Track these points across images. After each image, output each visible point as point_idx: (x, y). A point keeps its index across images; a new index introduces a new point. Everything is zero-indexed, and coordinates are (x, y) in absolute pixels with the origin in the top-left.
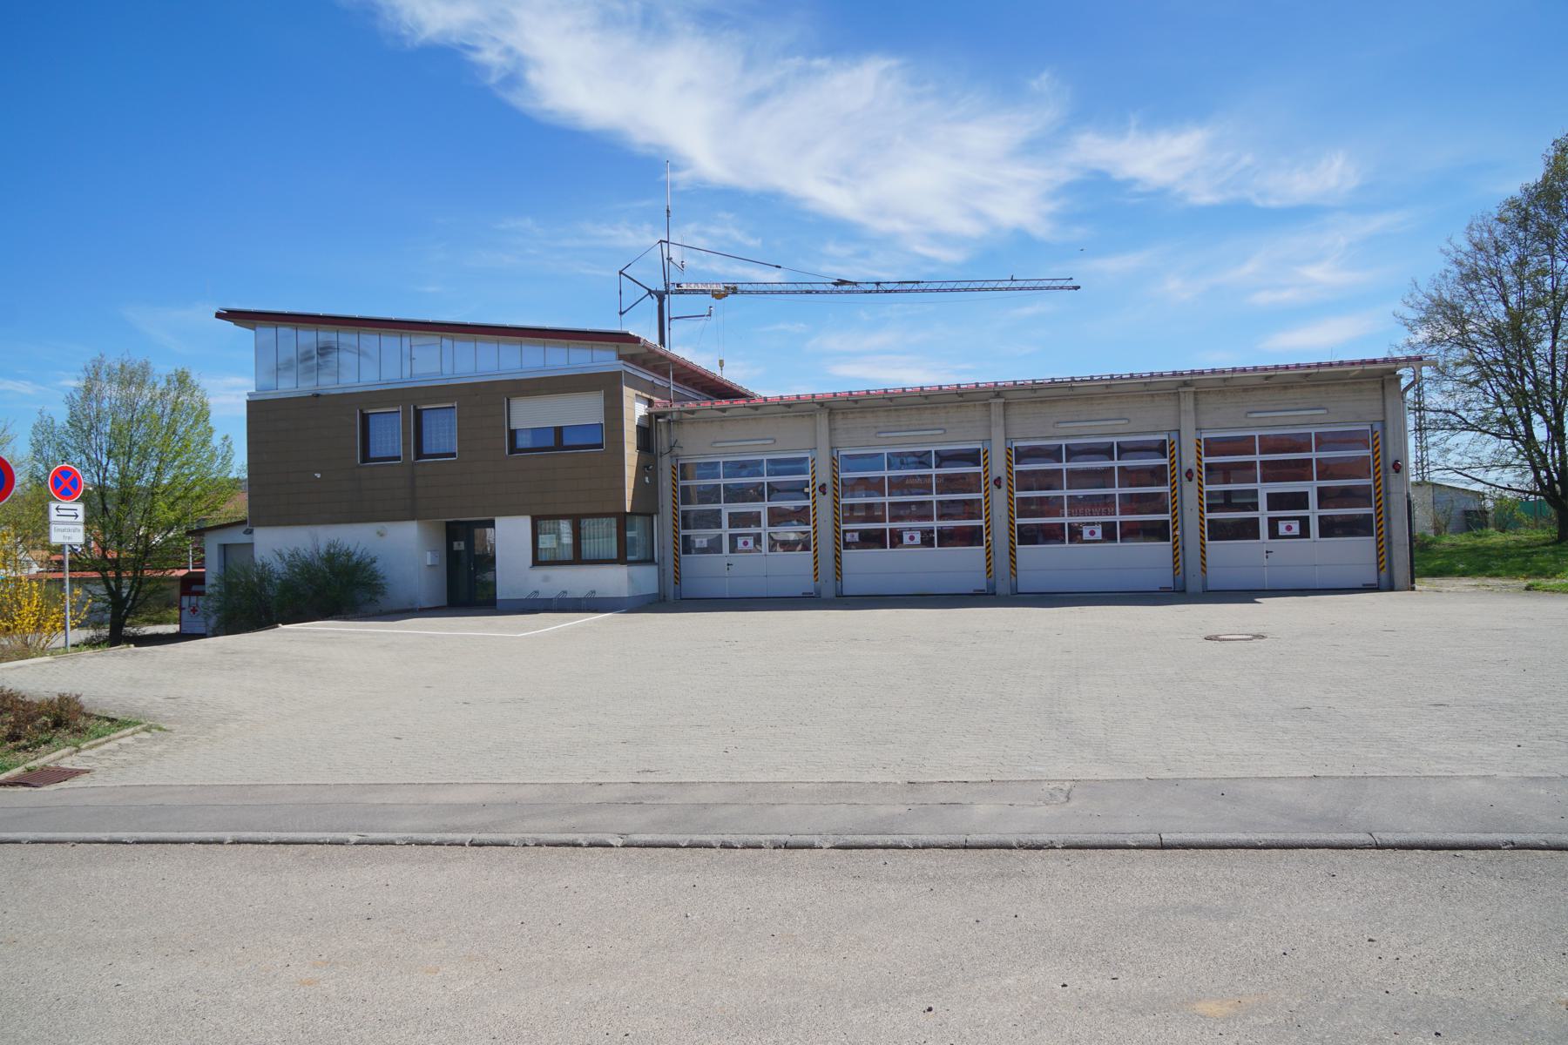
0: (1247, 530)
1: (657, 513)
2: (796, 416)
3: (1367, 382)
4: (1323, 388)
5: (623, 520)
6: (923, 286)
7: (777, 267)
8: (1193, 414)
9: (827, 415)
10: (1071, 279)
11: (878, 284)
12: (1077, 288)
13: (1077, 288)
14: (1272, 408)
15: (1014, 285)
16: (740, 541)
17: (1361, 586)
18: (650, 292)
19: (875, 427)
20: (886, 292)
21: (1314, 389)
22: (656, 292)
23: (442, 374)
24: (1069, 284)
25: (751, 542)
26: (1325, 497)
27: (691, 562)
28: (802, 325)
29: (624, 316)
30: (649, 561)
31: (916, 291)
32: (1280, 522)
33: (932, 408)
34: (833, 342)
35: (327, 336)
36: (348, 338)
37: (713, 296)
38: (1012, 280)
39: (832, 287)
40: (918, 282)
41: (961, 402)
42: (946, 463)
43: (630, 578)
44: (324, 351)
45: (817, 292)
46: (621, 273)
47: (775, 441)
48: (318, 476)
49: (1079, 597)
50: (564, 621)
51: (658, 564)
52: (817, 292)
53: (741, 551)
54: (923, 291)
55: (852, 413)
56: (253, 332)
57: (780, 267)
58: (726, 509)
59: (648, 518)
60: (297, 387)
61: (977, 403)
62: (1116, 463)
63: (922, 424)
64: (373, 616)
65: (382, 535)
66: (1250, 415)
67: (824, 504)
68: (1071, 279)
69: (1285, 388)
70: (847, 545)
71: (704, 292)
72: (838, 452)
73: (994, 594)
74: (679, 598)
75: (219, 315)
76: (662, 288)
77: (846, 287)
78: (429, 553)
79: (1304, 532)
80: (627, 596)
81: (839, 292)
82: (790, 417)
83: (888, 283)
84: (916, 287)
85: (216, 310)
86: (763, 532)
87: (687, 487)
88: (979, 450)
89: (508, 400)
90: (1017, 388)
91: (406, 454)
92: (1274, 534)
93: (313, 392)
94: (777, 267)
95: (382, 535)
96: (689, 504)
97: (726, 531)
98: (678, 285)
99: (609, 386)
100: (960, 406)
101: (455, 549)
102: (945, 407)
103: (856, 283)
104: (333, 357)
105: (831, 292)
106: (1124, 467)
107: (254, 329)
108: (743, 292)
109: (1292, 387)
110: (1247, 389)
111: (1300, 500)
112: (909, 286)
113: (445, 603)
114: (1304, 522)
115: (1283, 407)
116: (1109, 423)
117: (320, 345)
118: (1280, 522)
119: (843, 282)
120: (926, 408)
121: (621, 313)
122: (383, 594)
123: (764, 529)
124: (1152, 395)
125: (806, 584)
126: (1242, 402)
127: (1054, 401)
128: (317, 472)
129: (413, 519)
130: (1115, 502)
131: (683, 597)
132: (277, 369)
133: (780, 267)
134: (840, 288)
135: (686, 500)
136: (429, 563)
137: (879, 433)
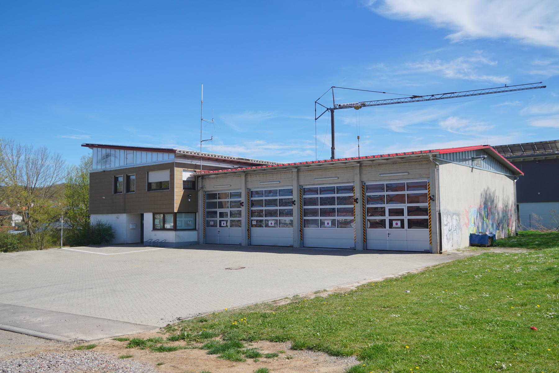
0: (382, 224)
1: (198, 212)
2: (237, 176)
3: (425, 160)
4: (407, 164)
5: (175, 215)
6: (456, 95)
7: (384, 93)
8: (359, 175)
9: (244, 176)
10: (541, 83)
11: (433, 96)
12: (545, 87)
13: (545, 87)
14: (388, 172)
15: (507, 89)
16: (394, 223)
17: (424, 251)
18: (328, 109)
19: (260, 180)
20: (437, 99)
21: (404, 164)
22: (330, 109)
23: (136, 163)
24: (540, 85)
25: (399, 223)
26: (411, 211)
27: (211, 230)
28: (518, 102)
29: (316, 120)
30: (195, 229)
31: (453, 97)
32: (393, 221)
33: (276, 173)
34: (535, 109)
35: (108, 151)
36: (113, 151)
37: (355, 108)
38: (506, 87)
39: (410, 99)
40: (453, 93)
41: (286, 170)
42: (233, 197)
43: (176, 235)
44: (108, 156)
45: (403, 102)
46: (316, 102)
47: (231, 186)
48: (104, 198)
49: (325, 250)
50: (146, 249)
51: (197, 230)
52: (403, 102)
53: (223, 227)
54: (457, 97)
55: (253, 175)
56: (92, 150)
57: (385, 93)
58: (388, 207)
59: (195, 214)
60: (110, 167)
61: (290, 171)
62: (336, 195)
63: (274, 179)
64: (113, 245)
65: (118, 218)
66: (215, 187)
67: (358, 208)
68: (541, 83)
69: (394, 163)
70: (252, 226)
71: (351, 107)
72: (302, 186)
73: (355, 249)
74: (205, 243)
75: (82, 146)
76: (332, 107)
77: (417, 99)
78: (131, 224)
79: (402, 226)
80: (174, 242)
81: (413, 101)
82: (235, 176)
83: (438, 95)
84: (453, 95)
85: (82, 144)
86: (386, 219)
87: (221, 202)
88: (427, 182)
89: (148, 173)
90: (536, 144)
91: (124, 191)
92: (391, 226)
93: (104, 170)
94: (384, 93)
95: (118, 218)
96: (223, 208)
97: (387, 218)
98: (339, 105)
99: (170, 167)
100: (285, 172)
101: (211, 224)
102: (280, 173)
103: (421, 97)
104: (109, 158)
105: (410, 102)
106: (339, 197)
107: (92, 149)
108: (368, 106)
109: (396, 163)
110: (394, 163)
111: (400, 212)
112: (449, 95)
113: (140, 242)
114: (402, 221)
115: (392, 172)
116: (330, 179)
117: (107, 154)
118: (393, 221)
119: (415, 97)
120: (274, 173)
121: (316, 119)
122: (114, 238)
123: (406, 217)
124: (347, 167)
125: (350, 244)
126: (378, 170)
127: (315, 170)
128: (104, 197)
129: (124, 213)
130: (335, 211)
131: (207, 243)
132: (97, 162)
133: (385, 93)
134: (414, 99)
135: (253, 205)
136: (131, 228)
137: (381, 174)
